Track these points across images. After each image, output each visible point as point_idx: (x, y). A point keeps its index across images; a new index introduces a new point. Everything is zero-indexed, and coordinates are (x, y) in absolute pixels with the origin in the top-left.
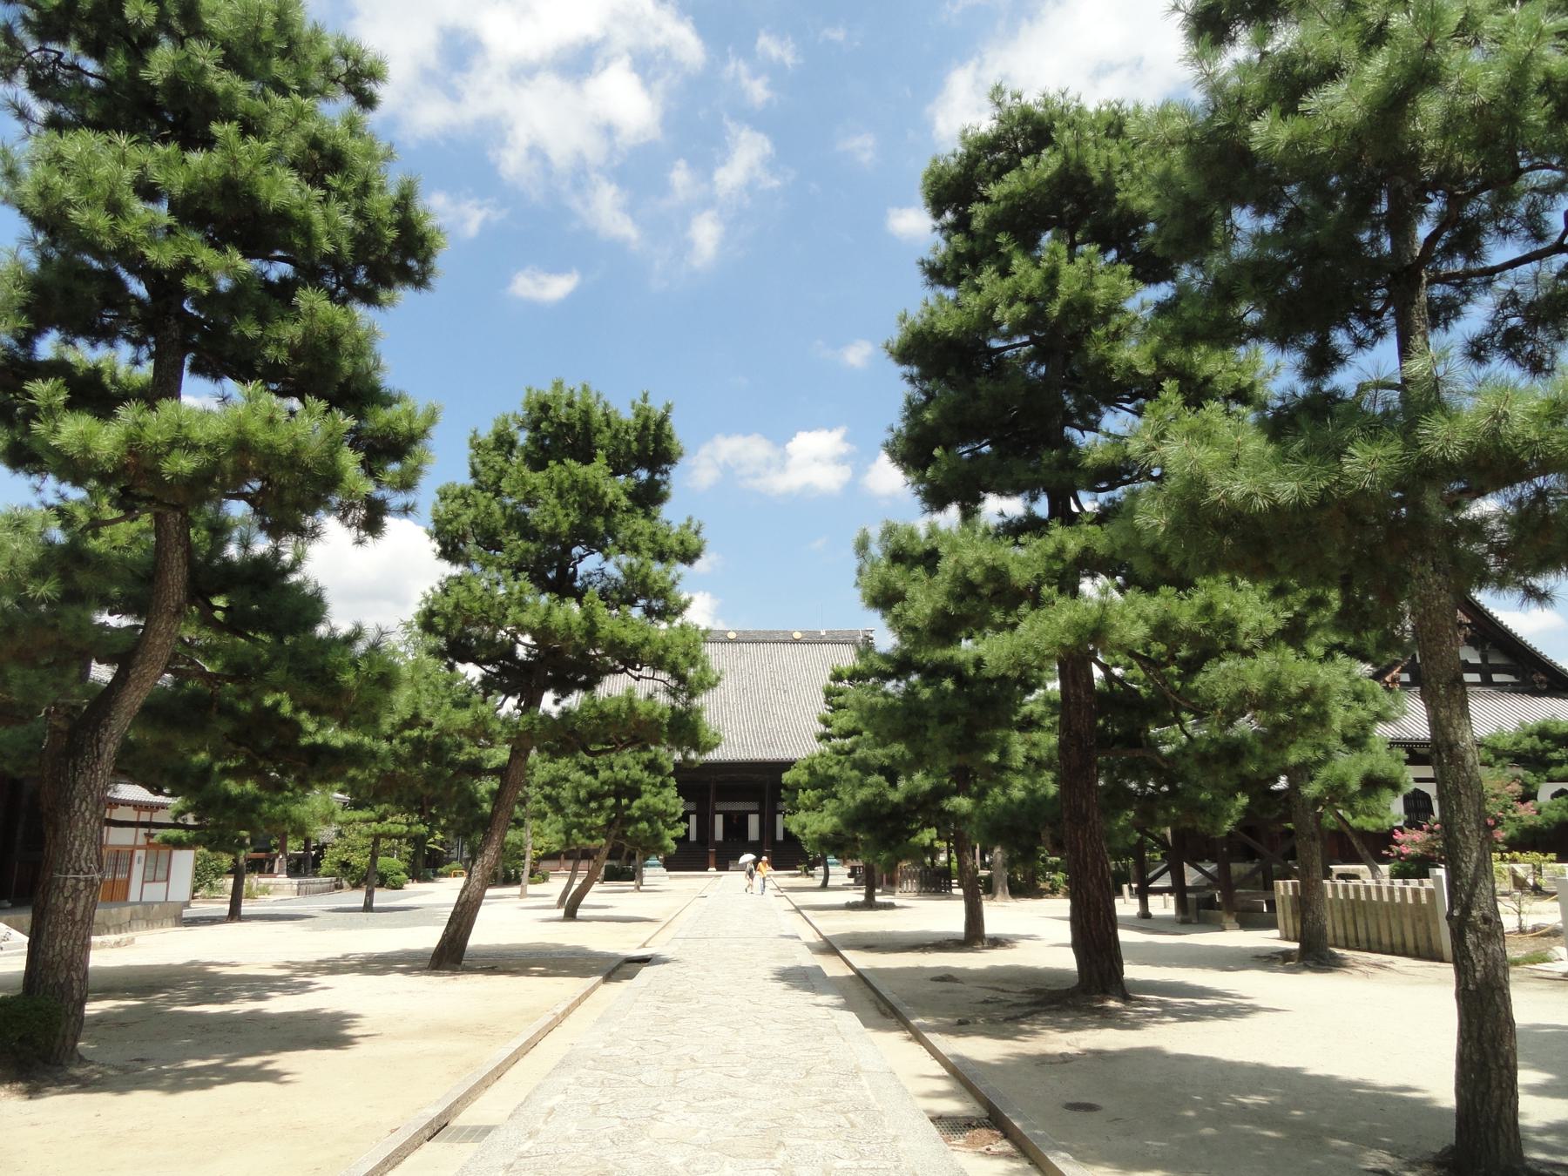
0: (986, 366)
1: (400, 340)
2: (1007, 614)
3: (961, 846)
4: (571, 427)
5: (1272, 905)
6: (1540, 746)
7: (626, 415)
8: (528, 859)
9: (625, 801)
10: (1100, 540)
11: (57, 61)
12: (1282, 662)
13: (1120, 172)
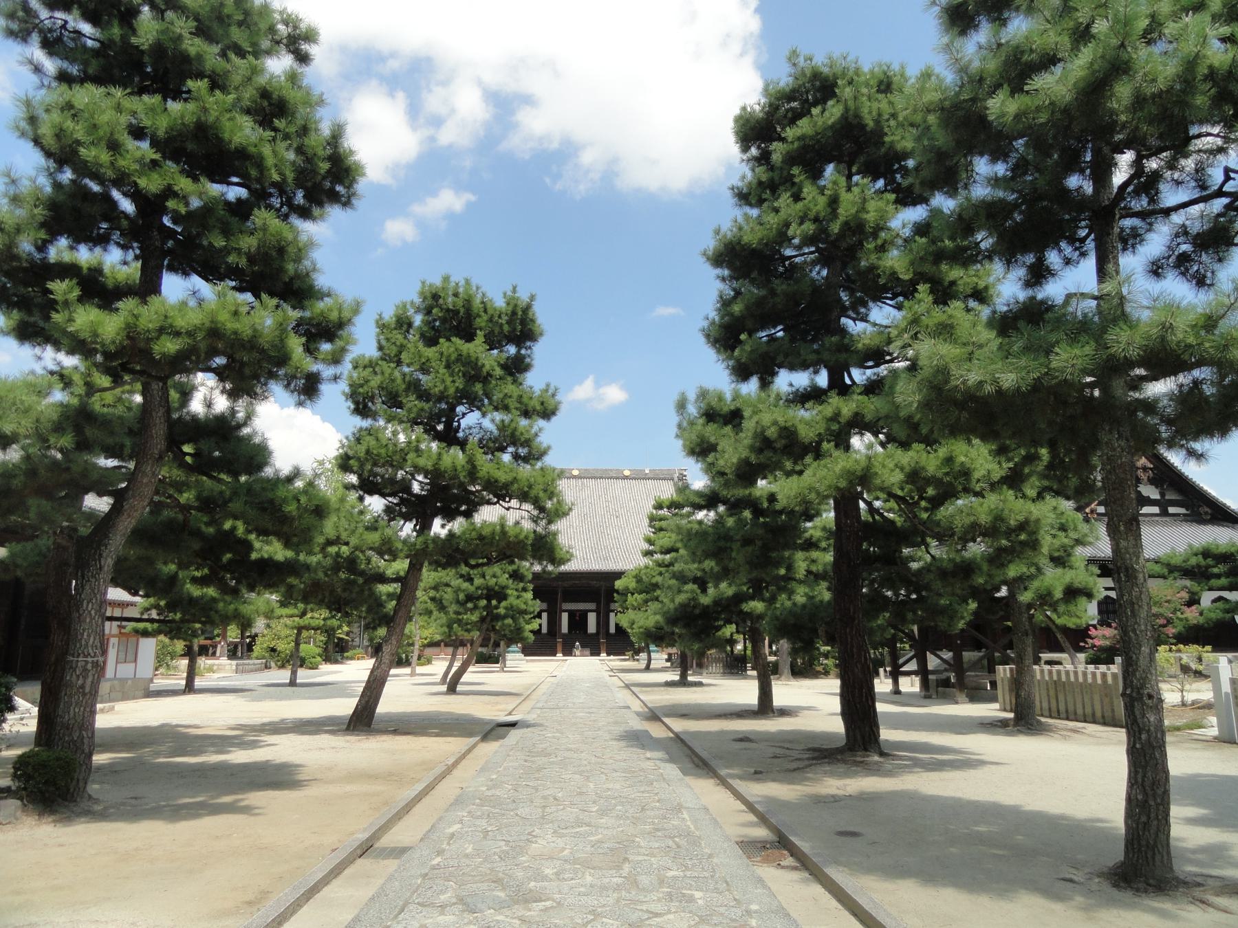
0: (781, 269)
1: (329, 246)
2: (795, 463)
3: (755, 637)
4: (456, 312)
5: (994, 684)
6: (1203, 563)
7: (500, 303)
8: (417, 647)
9: (494, 602)
10: (872, 406)
11: (64, 27)
12: (1004, 501)
13: (888, 120)
